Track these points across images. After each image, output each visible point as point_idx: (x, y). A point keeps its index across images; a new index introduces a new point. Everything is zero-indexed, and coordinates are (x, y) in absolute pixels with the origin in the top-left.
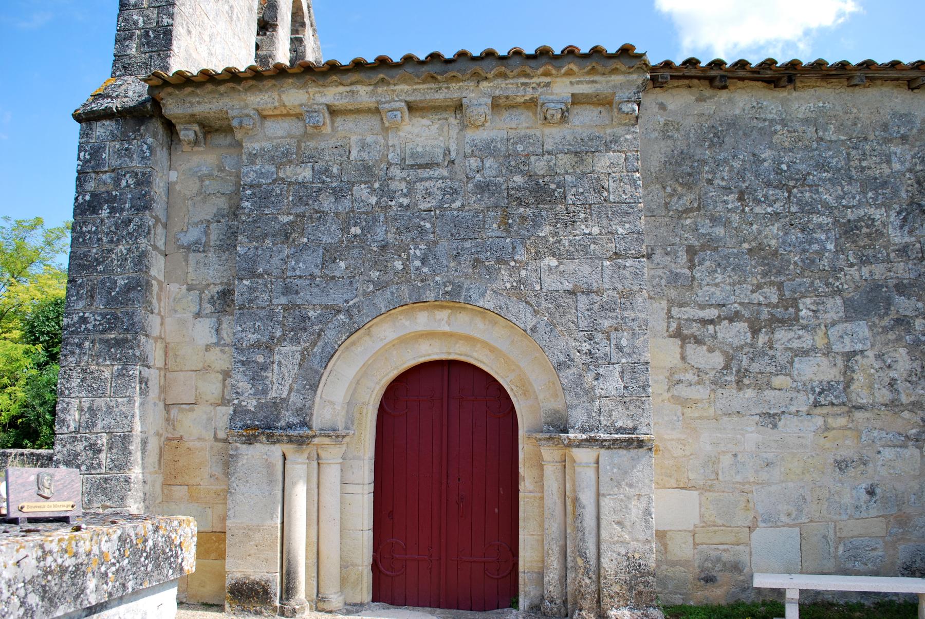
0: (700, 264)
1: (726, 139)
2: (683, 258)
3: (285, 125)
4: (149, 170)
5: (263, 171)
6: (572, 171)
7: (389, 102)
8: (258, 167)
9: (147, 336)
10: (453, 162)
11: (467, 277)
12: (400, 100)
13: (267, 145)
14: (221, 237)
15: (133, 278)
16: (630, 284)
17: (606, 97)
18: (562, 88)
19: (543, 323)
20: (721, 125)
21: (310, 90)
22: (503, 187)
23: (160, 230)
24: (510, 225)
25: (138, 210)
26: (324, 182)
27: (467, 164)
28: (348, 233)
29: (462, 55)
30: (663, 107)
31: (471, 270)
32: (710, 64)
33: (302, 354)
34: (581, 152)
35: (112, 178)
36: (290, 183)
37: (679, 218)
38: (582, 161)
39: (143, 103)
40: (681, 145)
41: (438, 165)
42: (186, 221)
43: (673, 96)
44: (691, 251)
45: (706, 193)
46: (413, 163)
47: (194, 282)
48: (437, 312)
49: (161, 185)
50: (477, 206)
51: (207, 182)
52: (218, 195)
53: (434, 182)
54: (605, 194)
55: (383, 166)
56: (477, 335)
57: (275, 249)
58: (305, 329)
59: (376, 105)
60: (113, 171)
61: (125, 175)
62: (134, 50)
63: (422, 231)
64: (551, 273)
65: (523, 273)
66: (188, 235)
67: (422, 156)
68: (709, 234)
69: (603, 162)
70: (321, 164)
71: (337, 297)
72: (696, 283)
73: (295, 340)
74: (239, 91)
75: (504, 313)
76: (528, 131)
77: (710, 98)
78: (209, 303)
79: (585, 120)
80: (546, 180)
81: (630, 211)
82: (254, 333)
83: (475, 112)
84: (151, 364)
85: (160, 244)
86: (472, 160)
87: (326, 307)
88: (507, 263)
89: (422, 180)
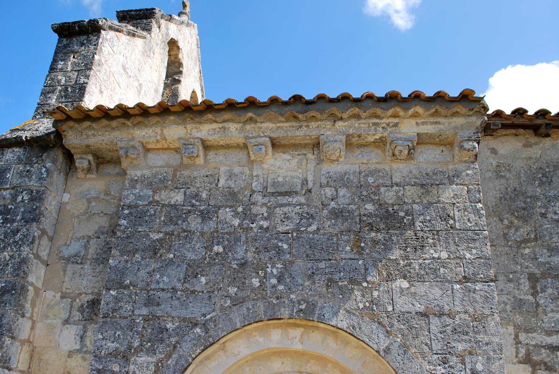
0: (543, 291)
1: (554, 179)
2: (526, 285)
3: (165, 157)
4: (43, 188)
5: (142, 194)
6: (419, 201)
7: (255, 138)
8: (137, 191)
9: (13, 338)
10: (310, 191)
11: (321, 296)
12: (265, 136)
13: (147, 173)
14: (99, 251)
15: (10, 282)
16: (482, 308)
17: (448, 138)
18: (409, 127)
19: (396, 345)
20: (548, 167)
21: (188, 126)
22: (356, 214)
23: (45, 241)
24: (362, 248)
25: (27, 222)
26: (193, 206)
27: (323, 192)
28: (211, 251)
29: (321, 98)
30: (494, 151)
31: (324, 289)
32: (536, 113)
33: (157, 366)
34: (427, 184)
35: (11, 194)
36: (164, 206)
37: (519, 247)
38: (428, 192)
39: (48, 135)
40: (514, 183)
41: (296, 193)
42: (70, 236)
43: (503, 142)
44: (532, 278)
45: (541, 226)
46: (274, 191)
47: (68, 291)
48: (290, 330)
49: (54, 203)
50: (331, 230)
51: (94, 204)
52: (102, 215)
53: (292, 208)
54: (451, 222)
55: (247, 193)
56: (329, 355)
57: (143, 263)
58: (162, 341)
59: (244, 141)
60: (13, 188)
61: (22, 192)
62: (54, 100)
63: (279, 251)
64: (403, 296)
65: (376, 294)
66: (70, 248)
67: (283, 185)
68: (548, 263)
69: (447, 194)
70: (193, 190)
71: (195, 310)
72: (540, 310)
73: (152, 351)
74: (128, 126)
75: (357, 333)
76: (378, 166)
77: (535, 144)
78: (79, 311)
79: (429, 158)
80: (395, 208)
81: (476, 237)
82: (113, 342)
83: (331, 148)
84: (14, 366)
85: (44, 254)
86: (327, 190)
87: (184, 320)
88: (360, 284)
89: (282, 205)
